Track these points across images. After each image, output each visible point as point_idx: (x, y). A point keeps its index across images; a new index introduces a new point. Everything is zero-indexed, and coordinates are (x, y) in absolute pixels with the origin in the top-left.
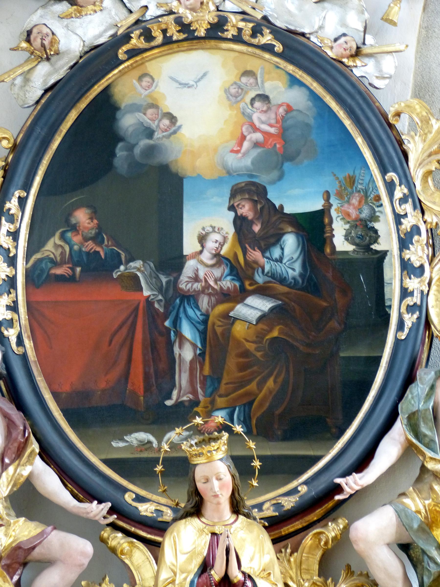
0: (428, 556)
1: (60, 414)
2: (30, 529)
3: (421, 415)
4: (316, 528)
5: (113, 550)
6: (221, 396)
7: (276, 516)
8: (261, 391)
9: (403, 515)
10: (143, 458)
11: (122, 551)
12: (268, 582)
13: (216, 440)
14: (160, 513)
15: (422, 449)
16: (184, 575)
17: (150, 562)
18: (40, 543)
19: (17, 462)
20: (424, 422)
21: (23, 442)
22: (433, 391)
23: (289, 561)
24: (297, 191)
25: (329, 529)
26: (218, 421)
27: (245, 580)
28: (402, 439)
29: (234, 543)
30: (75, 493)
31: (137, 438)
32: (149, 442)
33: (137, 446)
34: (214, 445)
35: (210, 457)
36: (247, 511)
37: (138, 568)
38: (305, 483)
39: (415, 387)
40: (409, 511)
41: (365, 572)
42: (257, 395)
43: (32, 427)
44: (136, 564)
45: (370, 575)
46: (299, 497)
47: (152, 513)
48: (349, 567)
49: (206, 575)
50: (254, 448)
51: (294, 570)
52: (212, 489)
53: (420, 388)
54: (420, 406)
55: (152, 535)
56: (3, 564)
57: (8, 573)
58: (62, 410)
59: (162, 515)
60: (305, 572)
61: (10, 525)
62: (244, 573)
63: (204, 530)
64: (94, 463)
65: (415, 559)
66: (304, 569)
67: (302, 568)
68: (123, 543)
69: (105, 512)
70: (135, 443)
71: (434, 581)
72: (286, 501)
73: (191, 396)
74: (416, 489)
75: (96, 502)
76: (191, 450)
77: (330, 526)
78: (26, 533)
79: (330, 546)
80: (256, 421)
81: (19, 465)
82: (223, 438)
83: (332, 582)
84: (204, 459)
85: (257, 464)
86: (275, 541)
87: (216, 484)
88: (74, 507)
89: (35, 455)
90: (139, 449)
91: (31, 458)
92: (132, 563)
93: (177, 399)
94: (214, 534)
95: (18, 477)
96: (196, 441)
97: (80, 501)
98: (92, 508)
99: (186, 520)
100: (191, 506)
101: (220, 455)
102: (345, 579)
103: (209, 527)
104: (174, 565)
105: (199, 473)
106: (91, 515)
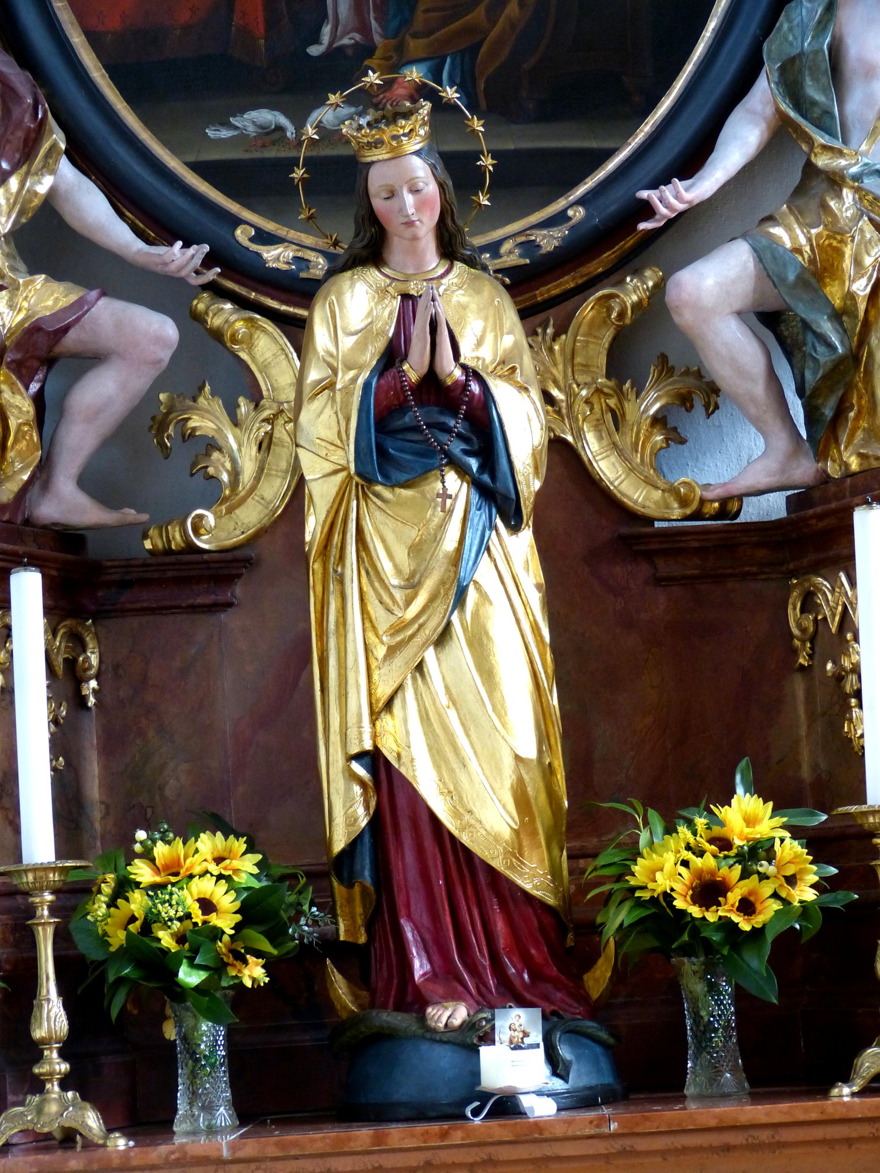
0: (815, 333)
1: (103, 75)
2: (56, 295)
3: (806, 62)
4: (602, 289)
5: (217, 335)
6: (415, 36)
7: (526, 265)
8: (495, 23)
9: (768, 256)
10: (269, 159)
11: (233, 335)
12: (511, 384)
13: (407, 115)
14: (304, 264)
15: (807, 130)
16: (352, 373)
17: (287, 356)
18: (78, 319)
19: (24, 168)
20: (811, 75)
21: (34, 129)
22: (832, 15)
23: (551, 350)
25: (627, 289)
26: (410, 79)
27: (467, 380)
28: (769, 111)
29: (446, 312)
30: (140, 228)
31: (255, 120)
32: (280, 129)
33: (255, 137)
34: (404, 125)
35: (396, 147)
36: (469, 253)
37: (265, 368)
38: (581, 202)
39: (797, 6)
40: (780, 248)
41: (696, 368)
42: (486, 34)
43: (52, 98)
44: (261, 360)
45: (703, 373)
46: (568, 228)
47: (288, 263)
48: (664, 359)
49: (393, 371)
50: (481, 131)
51: (561, 367)
52: (402, 209)
53: (807, 8)
54: (806, 44)
55: (290, 306)
56: (9, 359)
57: (20, 377)
58: (106, 67)
59: (308, 268)
60: (583, 370)
61: (18, 289)
62: (464, 367)
63: (387, 289)
64: (173, 170)
65: (789, 341)
66: (579, 364)
67: (575, 362)
68: (236, 321)
69: (198, 261)
70: (251, 129)
71: (823, 377)
72: (544, 237)
73: (358, 37)
74: (793, 208)
75: (179, 244)
76: (359, 135)
77: (629, 284)
78: (50, 303)
79: (628, 321)
80: (486, 82)
81: (28, 173)
82: (421, 111)
83: (632, 389)
84: (384, 152)
85: (487, 162)
86: (524, 314)
87: (409, 199)
88: (139, 251)
89: (59, 155)
90: (259, 143)
91: (51, 161)
92: (253, 358)
93: (331, 43)
94: (406, 297)
95: (27, 196)
96: (368, 118)
97: (149, 241)
98: (174, 255)
99: (353, 272)
100: (362, 243)
101: (414, 145)
102: (658, 378)
103: (398, 283)
104: (331, 355)
105: (376, 180)
106: (173, 267)
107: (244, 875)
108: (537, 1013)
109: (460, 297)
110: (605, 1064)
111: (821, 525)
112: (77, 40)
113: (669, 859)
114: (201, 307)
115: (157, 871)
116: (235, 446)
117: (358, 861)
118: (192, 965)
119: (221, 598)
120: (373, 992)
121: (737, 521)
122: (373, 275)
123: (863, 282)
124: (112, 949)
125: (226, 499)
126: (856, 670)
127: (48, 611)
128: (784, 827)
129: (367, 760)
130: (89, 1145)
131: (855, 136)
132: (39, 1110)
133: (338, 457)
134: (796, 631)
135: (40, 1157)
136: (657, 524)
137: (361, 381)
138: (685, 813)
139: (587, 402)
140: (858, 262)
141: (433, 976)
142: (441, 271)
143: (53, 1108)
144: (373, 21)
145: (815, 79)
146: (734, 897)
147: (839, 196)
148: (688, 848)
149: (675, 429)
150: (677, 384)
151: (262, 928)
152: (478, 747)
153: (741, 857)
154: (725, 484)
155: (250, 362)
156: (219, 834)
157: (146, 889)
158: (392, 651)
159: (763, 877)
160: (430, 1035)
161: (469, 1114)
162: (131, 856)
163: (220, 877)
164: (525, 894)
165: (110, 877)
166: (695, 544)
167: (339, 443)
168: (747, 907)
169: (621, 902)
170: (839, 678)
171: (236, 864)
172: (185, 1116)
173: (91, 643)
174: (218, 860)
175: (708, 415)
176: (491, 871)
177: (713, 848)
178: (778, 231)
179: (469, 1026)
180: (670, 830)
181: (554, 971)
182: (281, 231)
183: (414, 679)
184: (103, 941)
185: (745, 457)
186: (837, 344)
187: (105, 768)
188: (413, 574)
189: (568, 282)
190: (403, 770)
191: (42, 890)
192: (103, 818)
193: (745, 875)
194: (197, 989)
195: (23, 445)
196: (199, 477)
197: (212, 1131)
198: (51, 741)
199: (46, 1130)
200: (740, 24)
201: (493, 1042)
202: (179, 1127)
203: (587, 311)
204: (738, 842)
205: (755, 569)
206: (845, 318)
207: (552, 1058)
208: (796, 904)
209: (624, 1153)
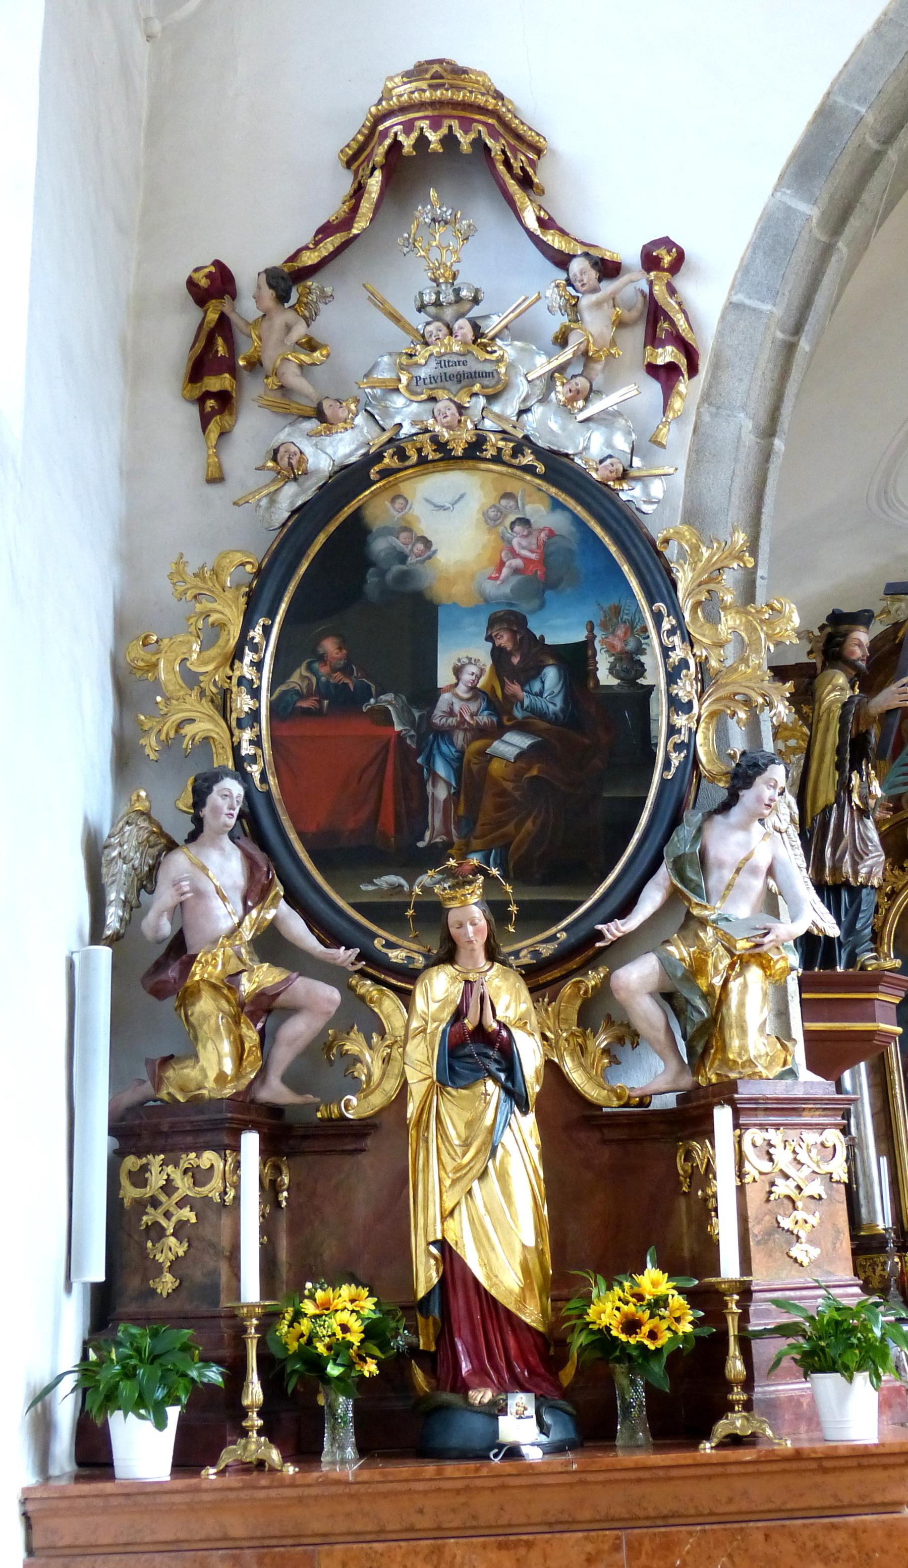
0: (692, 1005)
5: (362, 998)
9: (667, 963)
13: (470, 883)
16: (436, 1024)
19: (261, 905)
23: (546, 1010)
24: (559, 622)
28: (667, 884)
29: (489, 991)
32: (401, 886)
37: (388, 1017)
38: (565, 929)
42: (515, 837)
44: (386, 1012)
48: (609, 1017)
51: (552, 1020)
52: (466, 933)
62: (499, 1022)
69: (353, 958)
71: (697, 1031)
73: (445, 838)
75: (343, 948)
78: (271, 979)
79: (589, 996)
85: (513, 908)
86: (531, 991)
87: (470, 929)
89: (280, 898)
92: (382, 1012)
93: (430, 841)
94: (467, 982)
96: (449, 884)
97: (326, 946)
101: (474, 899)
105: (453, 918)
106: (339, 961)
107: (366, 1311)
108: (532, 1395)
109: (497, 982)
110: (571, 1426)
111: (695, 1113)
112: (293, 836)
113: (609, 1306)
114: (354, 982)
115: (317, 1306)
116: (369, 1060)
117: (431, 1303)
118: (335, 1363)
119: (358, 1146)
120: (438, 1380)
121: (650, 1108)
122: (449, 969)
123: (718, 978)
124: (290, 1353)
125: (364, 1090)
126: (715, 1196)
127: (262, 1152)
128: (674, 1288)
129: (439, 1245)
130: (272, 1470)
131: (713, 898)
132: (245, 1448)
133: (427, 1071)
134: (681, 1172)
135: (245, 1477)
136: (604, 1110)
137: (441, 1029)
138: (617, 1278)
139: (566, 1040)
140: (715, 967)
141: (473, 1372)
142: (487, 967)
143: (253, 1447)
144: (453, 830)
145: (691, 866)
146: (645, 1329)
147: (705, 931)
148: (620, 1299)
149: (615, 1056)
150: (616, 1031)
151: (375, 1342)
152: (501, 1239)
153: (649, 1306)
154: (642, 1088)
155: (379, 1013)
156: (353, 1285)
157: (311, 1318)
158: (454, 1182)
159: (662, 1318)
160: (470, 1407)
161: (492, 1457)
162: (302, 1297)
163: (353, 1311)
164: (527, 1325)
165: (290, 1309)
166: (626, 1121)
167: (427, 1062)
168: (653, 1335)
169: (581, 1331)
170: (705, 1200)
171: (362, 1303)
172: (328, 1452)
173: (285, 1171)
174: (352, 1301)
175: (633, 1048)
176: (508, 1311)
177: (634, 1300)
178: (671, 949)
179: (493, 1403)
180: (610, 1288)
181: (542, 1370)
182: (400, 942)
183: (466, 1198)
184: (285, 1347)
185: (653, 1071)
186: (705, 1012)
187: (290, 1243)
188: (467, 1139)
189: (557, 973)
190: (459, 1251)
191: (252, 1318)
192: (288, 1272)
193: (652, 1316)
194: (338, 1378)
195: (252, 1058)
196: (350, 1077)
197: (343, 1462)
198: (260, 1227)
199: (248, 1460)
200: (651, 837)
201: (506, 1414)
202: (325, 1458)
203: (567, 989)
204: (648, 1297)
205: (658, 1136)
206: (708, 998)
207: (540, 1423)
208: (681, 1334)
209: (583, 1482)
